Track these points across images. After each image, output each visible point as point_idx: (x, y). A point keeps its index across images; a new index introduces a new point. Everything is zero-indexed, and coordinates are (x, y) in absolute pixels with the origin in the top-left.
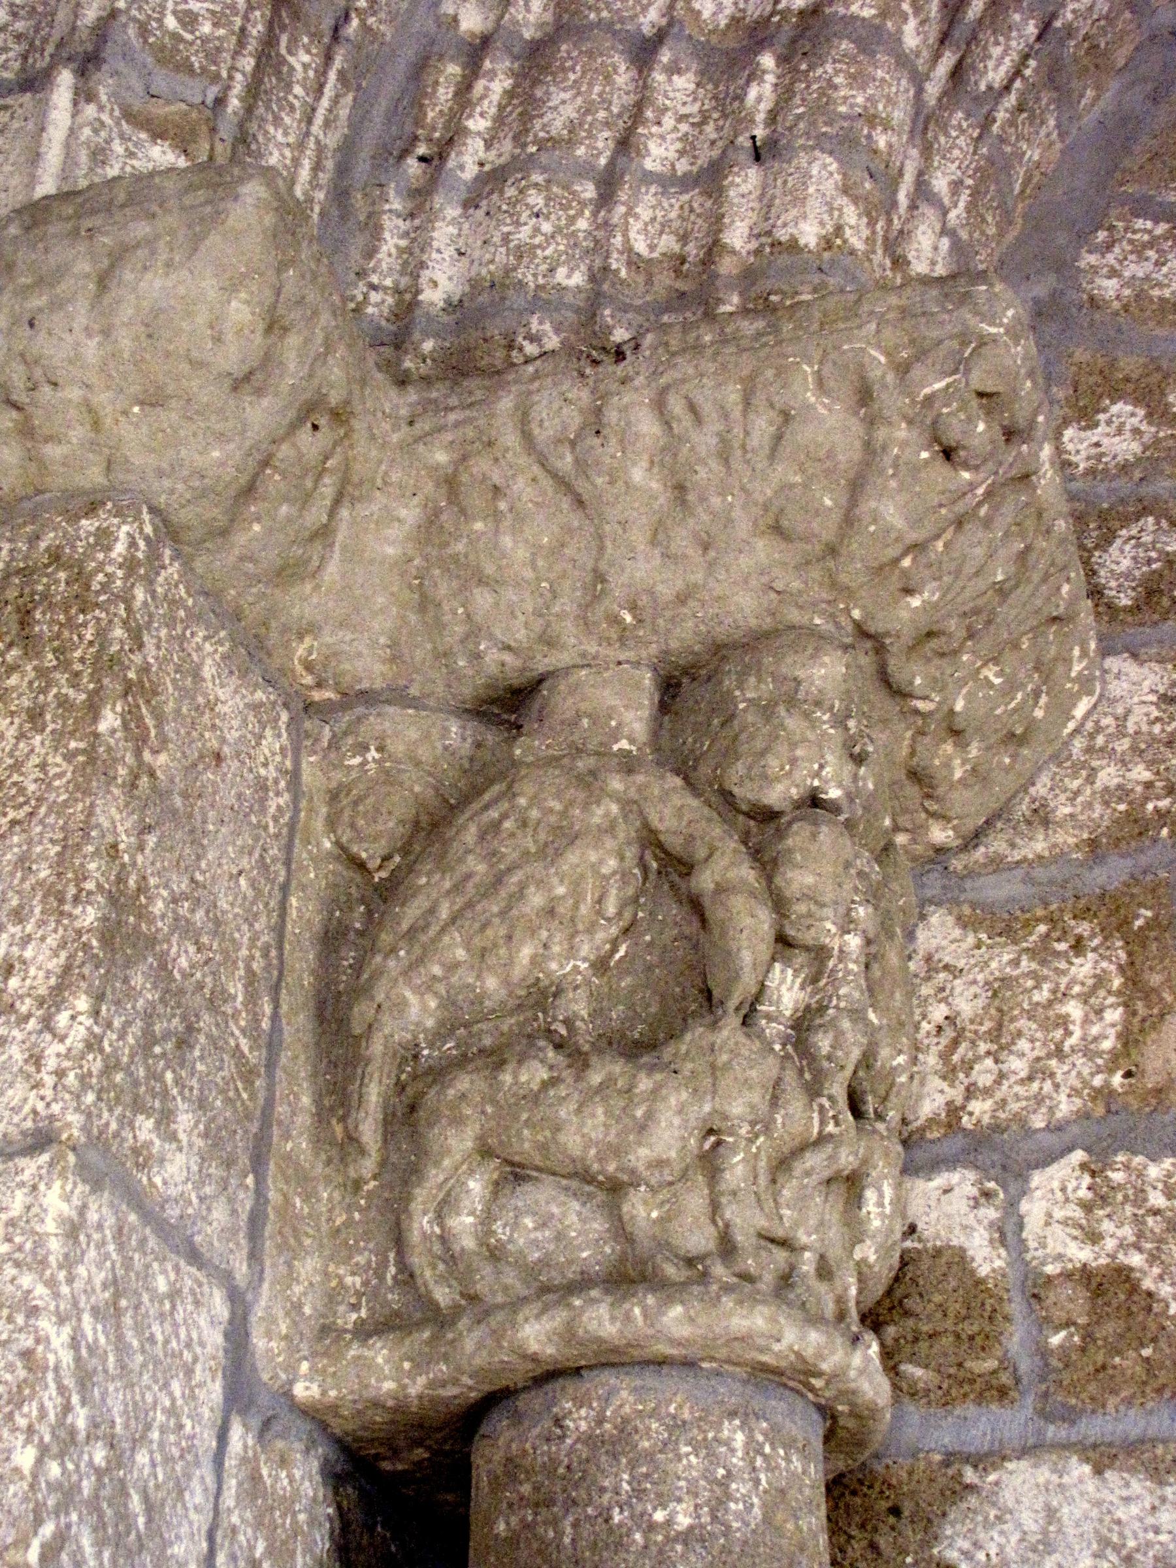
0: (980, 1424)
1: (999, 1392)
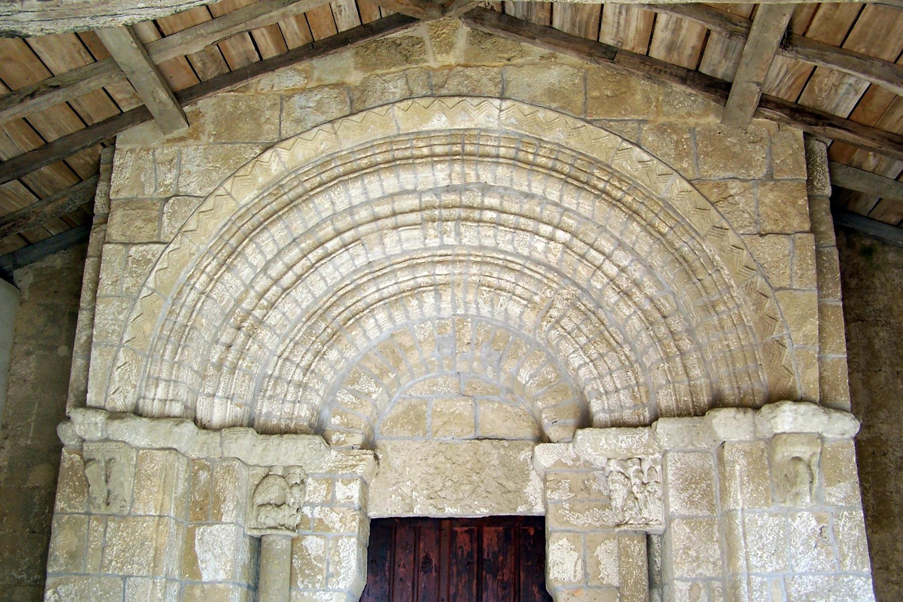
0: (308, 532)
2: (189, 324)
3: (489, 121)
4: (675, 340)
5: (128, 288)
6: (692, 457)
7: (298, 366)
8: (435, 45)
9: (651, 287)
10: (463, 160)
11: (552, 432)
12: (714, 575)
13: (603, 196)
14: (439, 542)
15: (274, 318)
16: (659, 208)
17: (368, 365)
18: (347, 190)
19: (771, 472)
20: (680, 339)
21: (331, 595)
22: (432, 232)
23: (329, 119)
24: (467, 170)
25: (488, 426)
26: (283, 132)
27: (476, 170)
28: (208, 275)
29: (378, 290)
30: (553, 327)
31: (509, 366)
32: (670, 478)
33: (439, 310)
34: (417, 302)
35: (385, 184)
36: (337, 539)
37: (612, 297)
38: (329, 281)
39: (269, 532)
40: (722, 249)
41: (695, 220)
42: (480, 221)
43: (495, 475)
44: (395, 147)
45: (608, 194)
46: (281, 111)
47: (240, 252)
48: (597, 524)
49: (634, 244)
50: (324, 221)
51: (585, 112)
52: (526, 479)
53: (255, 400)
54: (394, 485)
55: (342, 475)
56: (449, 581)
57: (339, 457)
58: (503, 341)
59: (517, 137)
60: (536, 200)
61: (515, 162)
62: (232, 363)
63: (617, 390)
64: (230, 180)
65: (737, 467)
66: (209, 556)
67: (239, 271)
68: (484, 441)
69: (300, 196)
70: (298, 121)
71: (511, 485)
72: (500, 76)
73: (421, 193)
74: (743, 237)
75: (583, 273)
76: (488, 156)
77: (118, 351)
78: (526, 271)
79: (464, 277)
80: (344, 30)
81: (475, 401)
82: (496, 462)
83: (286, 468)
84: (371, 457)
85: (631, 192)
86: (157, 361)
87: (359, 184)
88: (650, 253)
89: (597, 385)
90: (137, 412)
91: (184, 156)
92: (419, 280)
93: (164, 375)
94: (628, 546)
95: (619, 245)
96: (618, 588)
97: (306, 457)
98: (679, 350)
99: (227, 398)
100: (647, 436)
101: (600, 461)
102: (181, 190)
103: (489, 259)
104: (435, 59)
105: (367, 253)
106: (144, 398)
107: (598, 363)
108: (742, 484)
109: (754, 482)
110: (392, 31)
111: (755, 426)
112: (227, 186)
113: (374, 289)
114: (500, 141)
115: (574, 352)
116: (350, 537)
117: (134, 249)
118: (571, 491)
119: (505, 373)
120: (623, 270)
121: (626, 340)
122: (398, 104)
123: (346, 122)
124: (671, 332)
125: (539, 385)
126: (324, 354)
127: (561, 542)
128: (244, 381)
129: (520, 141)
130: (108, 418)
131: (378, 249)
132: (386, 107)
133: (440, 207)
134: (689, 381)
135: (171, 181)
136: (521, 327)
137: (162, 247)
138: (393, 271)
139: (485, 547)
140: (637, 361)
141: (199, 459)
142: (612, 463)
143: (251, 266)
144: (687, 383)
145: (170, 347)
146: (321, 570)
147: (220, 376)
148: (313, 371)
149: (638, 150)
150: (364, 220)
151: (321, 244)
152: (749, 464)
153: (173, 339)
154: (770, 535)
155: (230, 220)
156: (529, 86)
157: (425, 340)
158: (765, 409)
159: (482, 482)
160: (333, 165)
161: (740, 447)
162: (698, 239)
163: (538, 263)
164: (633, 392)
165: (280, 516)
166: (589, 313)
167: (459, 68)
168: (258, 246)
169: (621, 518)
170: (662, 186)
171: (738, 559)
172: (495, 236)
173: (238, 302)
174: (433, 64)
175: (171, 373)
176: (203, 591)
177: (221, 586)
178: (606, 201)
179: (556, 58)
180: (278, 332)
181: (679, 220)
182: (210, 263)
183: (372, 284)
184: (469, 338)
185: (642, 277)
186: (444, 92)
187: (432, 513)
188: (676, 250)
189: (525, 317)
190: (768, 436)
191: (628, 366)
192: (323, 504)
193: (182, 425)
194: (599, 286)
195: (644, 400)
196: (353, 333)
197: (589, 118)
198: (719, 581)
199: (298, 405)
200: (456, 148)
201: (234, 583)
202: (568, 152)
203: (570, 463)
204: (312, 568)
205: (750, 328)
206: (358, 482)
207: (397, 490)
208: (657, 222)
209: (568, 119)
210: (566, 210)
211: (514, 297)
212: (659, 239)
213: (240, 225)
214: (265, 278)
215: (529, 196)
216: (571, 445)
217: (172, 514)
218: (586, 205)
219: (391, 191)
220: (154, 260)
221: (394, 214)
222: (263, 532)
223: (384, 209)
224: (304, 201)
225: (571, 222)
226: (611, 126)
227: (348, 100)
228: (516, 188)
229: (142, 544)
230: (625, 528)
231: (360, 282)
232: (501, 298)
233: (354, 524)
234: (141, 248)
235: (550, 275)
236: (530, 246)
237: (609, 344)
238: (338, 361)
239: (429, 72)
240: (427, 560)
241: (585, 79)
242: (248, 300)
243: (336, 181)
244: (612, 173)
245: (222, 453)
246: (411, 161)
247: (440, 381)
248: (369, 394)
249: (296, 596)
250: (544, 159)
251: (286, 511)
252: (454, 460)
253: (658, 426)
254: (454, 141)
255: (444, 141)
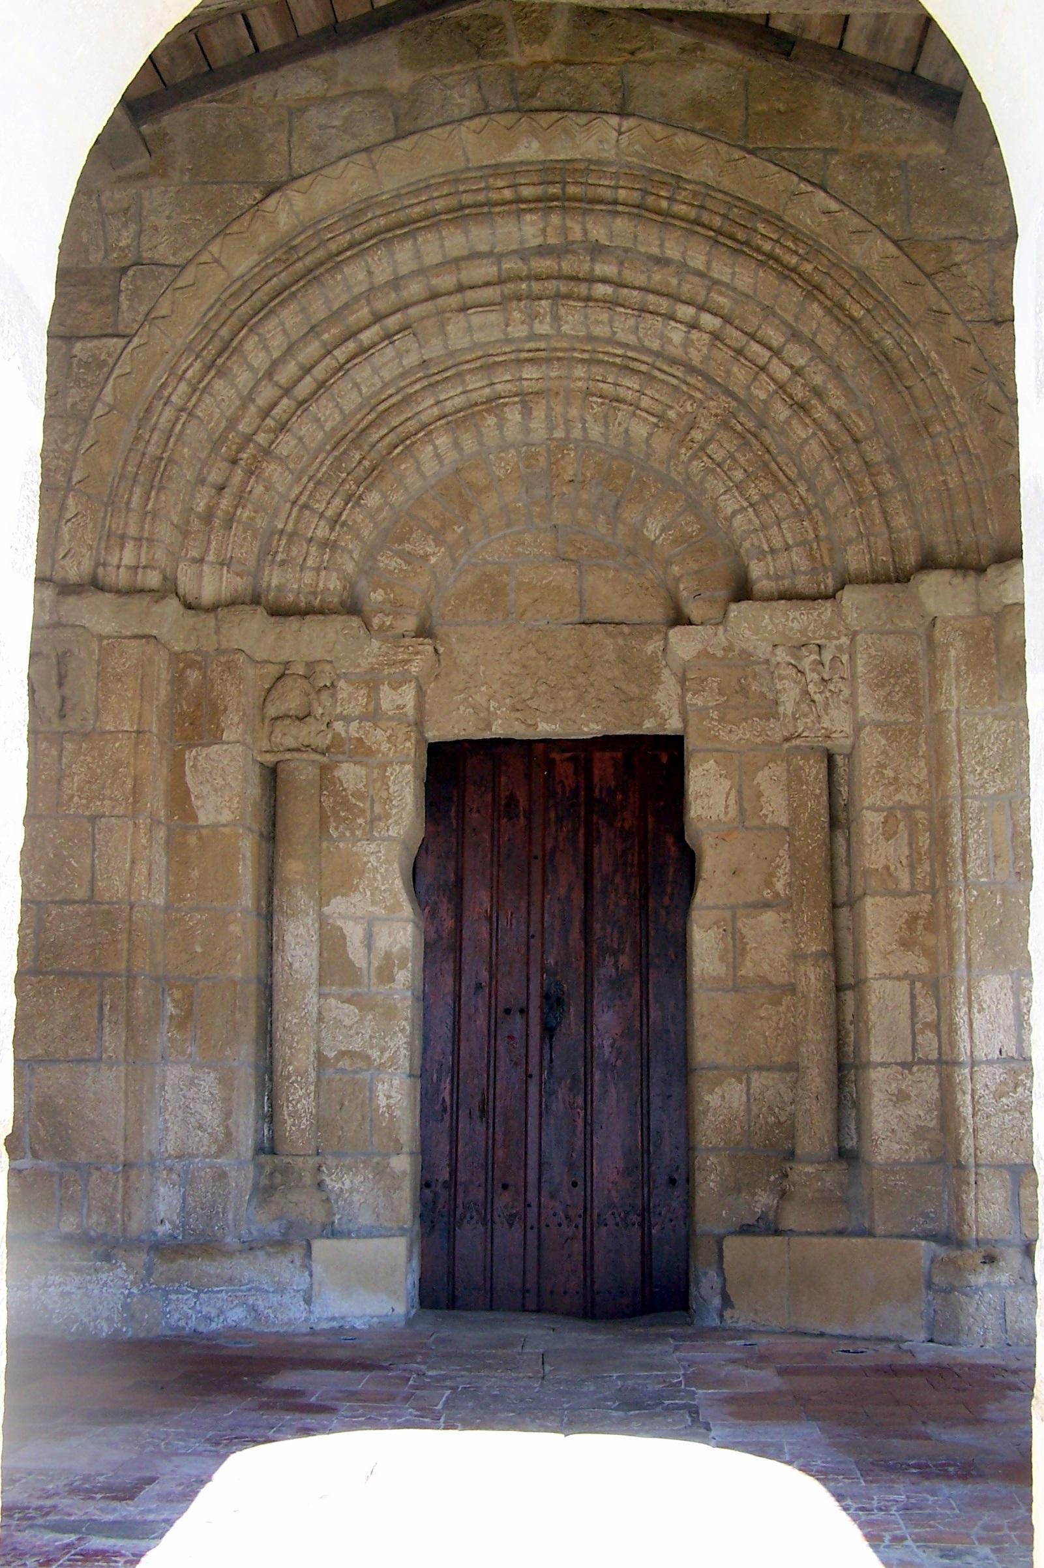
0: (340, 757)
1: (343, 753)
2: (165, 455)
3: (603, 150)
4: (871, 475)
5: (74, 404)
6: (891, 641)
7: (322, 515)
8: (521, 30)
9: (838, 398)
10: (564, 208)
11: (694, 610)
12: (918, 803)
13: (771, 262)
14: (528, 776)
15: (286, 445)
16: (851, 282)
17: (424, 514)
18: (392, 254)
19: (998, 660)
20: (879, 473)
21: (378, 845)
22: (517, 315)
23: (363, 146)
24: (569, 223)
25: (599, 604)
26: (295, 166)
27: (583, 223)
28: (190, 384)
29: (438, 403)
30: (695, 457)
31: (631, 514)
32: (861, 669)
33: (527, 431)
34: (495, 420)
35: (446, 244)
36: (384, 767)
37: (782, 412)
38: (364, 390)
39: (288, 756)
40: (939, 343)
41: (903, 300)
42: (588, 299)
43: (610, 675)
44: (461, 188)
45: (777, 260)
46: (290, 134)
47: (235, 349)
48: (759, 740)
49: (815, 334)
50: (356, 299)
51: (746, 136)
52: (655, 680)
53: (259, 567)
54: (461, 692)
55: (389, 674)
56: (545, 829)
57: (384, 649)
58: (623, 477)
59: (645, 173)
60: (672, 269)
61: (640, 211)
62: (227, 513)
63: (787, 548)
64: (218, 240)
65: (953, 653)
66: (205, 789)
67: (236, 377)
68: (595, 626)
69: (322, 263)
70: (317, 149)
71: (634, 690)
72: (619, 78)
73: (500, 258)
74: (970, 326)
75: (740, 376)
76: (600, 202)
77: (66, 497)
78: (656, 373)
79: (565, 382)
80: (381, 4)
81: (579, 568)
82: (611, 656)
83: (310, 665)
84: (430, 649)
85: (811, 257)
86: (120, 511)
87: (409, 245)
88: (837, 348)
89: (760, 540)
90: (96, 584)
91: (146, 203)
92: (499, 387)
93: (132, 531)
94: (801, 768)
95: (793, 335)
96: (786, 829)
97: (339, 647)
98: (877, 489)
99: (222, 564)
100: (829, 613)
101: (762, 650)
102: (144, 255)
103: (601, 356)
104: (522, 53)
105: (420, 346)
106: (105, 565)
107: (761, 507)
108: (958, 675)
109: (974, 673)
110: (454, 7)
111: (978, 595)
112: (215, 248)
113: (432, 402)
114: (618, 181)
115: (725, 493)
116: (403, 763)
117: (78, 346)
118: (721, 693)
119: (624, 524)
120: (797, 372)
121: (801, 474)
122: (467, 123)
123: (389, 151)
124: (866, 463)
125: (676, 542)
126: (360, 497)
127: (706, 766)
128: (245, 538)
129: (648, 178)
130: (59, 594)
131: (436, 342)
132: (448, 128)
133: (528, 278)
134: (890, 533)
135: (129, 241)
136: (648, 456)
137: (121, 342)
138: (459, 375)
139: (596, 780)
140: (816, 506)
141: (184, 652)
142: (779, 651)
143: (251, 367)
144: (886, 536)
145: (138, 490)
146: (363, 811)
147: (210, 531)
148: (344, 524)
149: (822, 194)
150: (416, 298)
151: (353, 335)
152: (968, 649)
153: (141, 478)
154: (993, 744)
155: (218, 299)
156: (663, 95)
157: (507, 476)
158: (992, 571)
159: (592, 685)
160: (370, 215)
161: (957, 624)
162: (906, 326)
163: (673, 361)
164: (811, 549)
165: (303, 733)
166: (749, 435)
167: (558, 67)
168: (262, 340)
169: (792, 730)
170: (857, 250)
171: (950, 778)
172: (611, 321)
173: (233, 422)
174: (517, 59)
175: (142, 528)
176: (200, 838)
177: (227, 830)
178: (774, 270)
179: (703, 50)
180: (291, 466)
181: (880, 299)
182: (191, 365)
183: (428, 393)
184: (571, 473)
185: (825, 382)
186: (536, 103)
187: (519, 731)
188: (875, 343)
189: (655, 443)
190: (997, 609)
191: (802, 513)
192: (362, 718)
193: (164, 602)
194: (763, 396)
195: (827, 561)
196: (403, 467)
197: (751, 146)
198: (924, 809)
199: (323, 573)
200: (554, 190)
201: (243, 826)
202: (719, 196)
203: (720, 653)
204: (350, 808)
205: (977, 457)
206: (413, 685)
207: (466, 699)
208: (848, 302)
209: (720, 146)
210: (716, 282)
211: (638, 412)
212: (850, 327)
213: (233, 307)
214: (270, 387)
215: (661, 261)
216: (721, 628)
217: (155, 730)
218: (744, 276)
219: (456, 253)
220: (111, 361)
221: (461, 288)
222: (280, 757)
223: (446, 281)
224: (327, 271)
225: (722, 300)
226: (783, 159)
227: (391, 115)
228: (642, 249)
229: (115, 771)
230: (797, 742)
231: (411, 390)
232: (620, 414)
233: (408, 744)
234: (90, 345)
235: (691, 380)
236: (662, 337)
237: (776, 480)
238: (379, 509)
239: (513, 73)
240: (512, 800)
241: (746, 84)
242: (247, 419)
243: (375, 240)
244: (785, 229)
245: (219, 644)
246: (486, 209)
247: (528, 538)
248: (425, 557)
249: (328, 848)
250: (684, 207)
251: (312, 726)
252: (550, 655)
253: (845, 598)
254: (551, 178)
255: (535, 179)
